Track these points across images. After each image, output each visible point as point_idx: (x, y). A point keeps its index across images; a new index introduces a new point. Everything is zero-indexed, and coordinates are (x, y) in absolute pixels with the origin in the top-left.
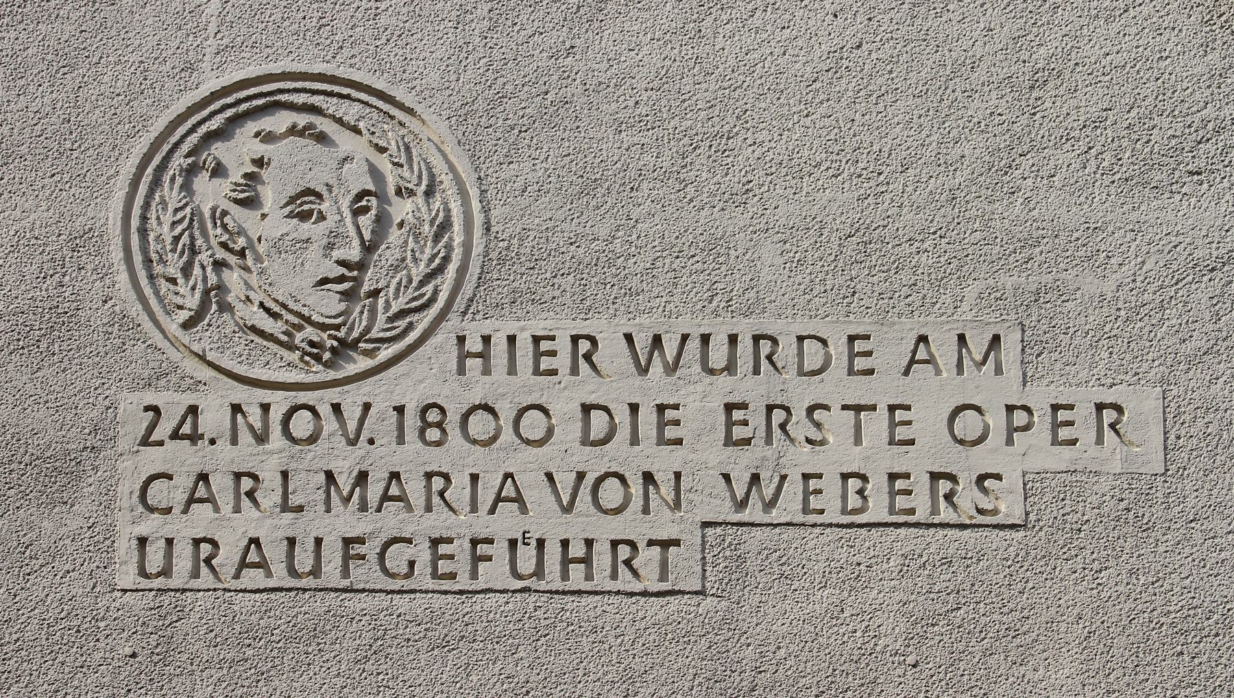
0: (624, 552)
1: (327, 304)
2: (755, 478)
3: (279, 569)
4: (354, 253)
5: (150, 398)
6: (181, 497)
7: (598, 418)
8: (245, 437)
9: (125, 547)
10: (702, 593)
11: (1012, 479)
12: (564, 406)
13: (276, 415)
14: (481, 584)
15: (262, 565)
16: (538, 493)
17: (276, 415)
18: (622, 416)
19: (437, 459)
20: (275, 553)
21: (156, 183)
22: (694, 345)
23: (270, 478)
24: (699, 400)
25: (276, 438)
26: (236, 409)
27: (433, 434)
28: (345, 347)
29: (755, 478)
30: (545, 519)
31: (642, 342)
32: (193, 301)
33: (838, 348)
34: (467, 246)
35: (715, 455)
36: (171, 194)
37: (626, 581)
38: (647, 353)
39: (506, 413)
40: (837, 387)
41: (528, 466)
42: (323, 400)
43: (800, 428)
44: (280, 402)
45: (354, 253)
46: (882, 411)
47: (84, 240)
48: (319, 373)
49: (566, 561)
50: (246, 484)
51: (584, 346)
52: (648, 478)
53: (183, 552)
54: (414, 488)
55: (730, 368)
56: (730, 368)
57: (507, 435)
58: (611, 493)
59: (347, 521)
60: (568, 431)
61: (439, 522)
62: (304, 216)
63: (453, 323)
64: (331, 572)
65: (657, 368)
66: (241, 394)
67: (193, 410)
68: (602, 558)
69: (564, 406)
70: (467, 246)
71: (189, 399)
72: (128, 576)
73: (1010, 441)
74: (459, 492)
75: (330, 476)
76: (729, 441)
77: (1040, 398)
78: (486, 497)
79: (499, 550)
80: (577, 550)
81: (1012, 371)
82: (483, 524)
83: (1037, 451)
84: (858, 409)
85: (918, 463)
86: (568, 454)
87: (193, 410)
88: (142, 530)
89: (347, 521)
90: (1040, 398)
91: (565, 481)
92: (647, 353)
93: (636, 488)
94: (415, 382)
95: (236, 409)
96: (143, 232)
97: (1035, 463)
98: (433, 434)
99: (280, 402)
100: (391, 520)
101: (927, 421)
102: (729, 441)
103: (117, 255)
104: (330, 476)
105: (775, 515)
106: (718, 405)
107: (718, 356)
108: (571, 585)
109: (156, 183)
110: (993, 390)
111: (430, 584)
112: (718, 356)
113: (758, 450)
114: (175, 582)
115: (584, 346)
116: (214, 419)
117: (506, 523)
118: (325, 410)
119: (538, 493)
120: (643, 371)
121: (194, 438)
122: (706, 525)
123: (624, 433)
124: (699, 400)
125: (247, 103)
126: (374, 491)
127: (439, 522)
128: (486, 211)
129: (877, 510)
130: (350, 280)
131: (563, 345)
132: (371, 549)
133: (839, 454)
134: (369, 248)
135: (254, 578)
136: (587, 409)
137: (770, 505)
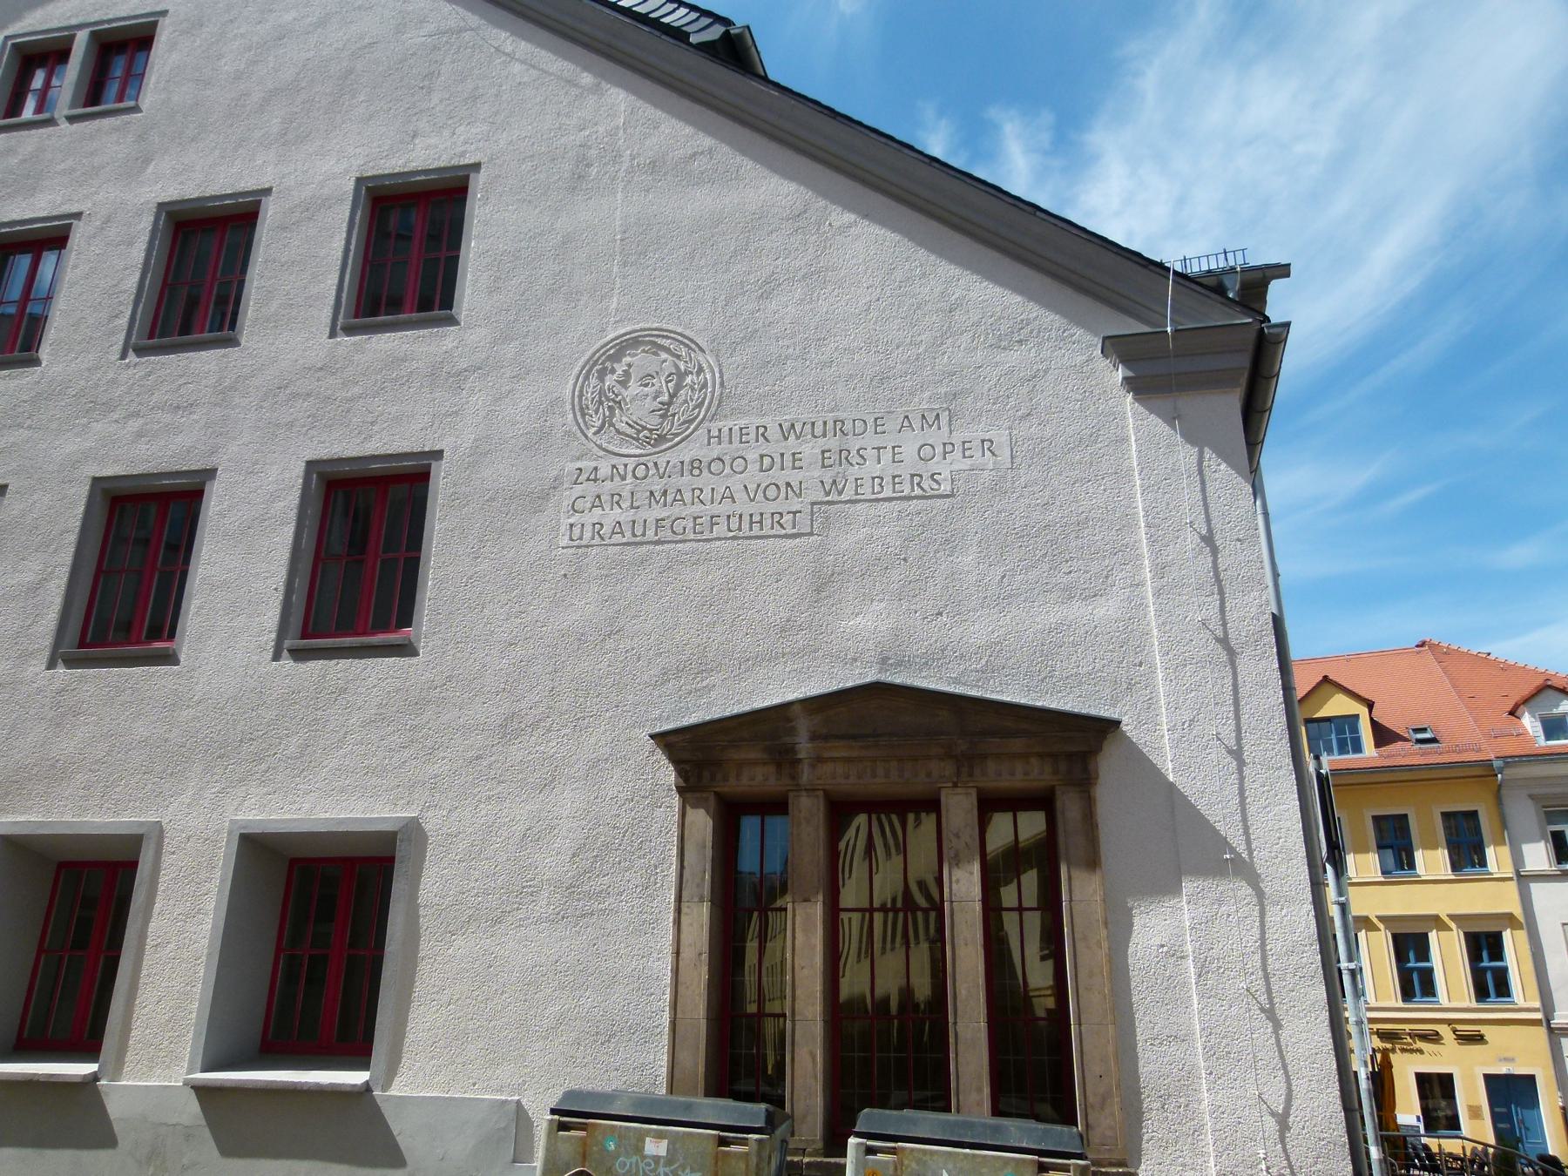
0: (777, 518)
1: (652, 422)
2: (834, 482)
3: (628, 534)
4: (666, 398)
5: (579, 465)
6: (589, 505)
7: (767, 461)
8: (617, 479)
9: (563, 528)
10: (811, 534)
11: (946, 474)
12: (752, 456)
13: (630, 468)
14: (715, 535)
15: (622, 533)
16: (740, 496)
17: (630, 468)
18: (777, 459)
19: (698, 482)
20: (627, 529)
21: (587, 378)
22: (808, 426)
23: (626, 494)
24: (810, 450)
25: (629, 479)
26: (614, 466)
27: (696, 472)
28: (662, 438)
29: (834, 482)
30: (743, 506)
31: (786, 426)
32: (598, 424)
33: (870, 422)
34: (713, 392)
35: (817, 473)
36: (593, 381)
37: (778, 531)
38: (787, 431)
39: (727, 459)
40: (870, 440)
41: (736, 484)
42: (650, 461)
43: (855, 459)
44: (631, 462)
45: (666, 398)
46: (889, 448)
47: (557, 401)
48: (650, 449)
49: (751, 523)
50: (616, 498)
51: (761, 430)
52: (788, 484)
53: (588, 528)
54: (687, 496)
55: (824, 435)
56: (824, 435)
57: (727, 470)
58: (772, 492)
59: (659, 512)
60: (753, 468)
61: (697, 509)
62: (646, 385)
63: (706, 424)
64: (650, 533)
65: (792, 437)
66: (616, 460)
67: (596, 469)
68: (767, 522)
69: (752, 456)
70: (713, 392)
71: (594, 464)
72: (565, 541)
73: (123, 356)
74: (706, 496)
75: (652, 493)
76: (823, 466)
77: (957, 438)
78: (718, 497)
79: (723, 520)
80: (756, 518)
81: (945, 429)
82: (717, 509)
83: (957, 462)
84: (879, 449)
85: (905, 471)
86: (753, 476)
87: (596, 469)
88: (571, 521)
89: (659, 512)
90: (957, 438)
91: (752, 487)
92: (787, 431)
93: (783, 489)
94: (687, 453)
95: (614, 466)
96: (581, 396)
97: (955, 467)
98: (696, 472)
99: (631, 462)
100: (677, 510)
101: (909, 451)
102: (823, 466)
103: (568, 407)
104: (652, 493)
105: (844, 497)
106: (818, 451)
107: (818, 430)
108: (753, 533)
109: (587, 378)
110: (937, 436)
111: (692, 536)
112: (818, 430)
113: (837, 469)
114: (584, 542)
115: (761, 430)
116: (604, 470)
117: (725, 508)
118: (650, 465)
119: (740, 496)
120: (786, 439)
121: (595, 480)
122: (813, 504)
123: (777, 465)
124: (810, 450)
125: (630, 343)
126: (669, 498)
127: (697, 509)
128: (721, 377)
129: (887, 493)
130: (665, 411)
131: (752, 430)
132: (667, 523)
133: (872, 468)
134: (672, 396)
135: (617, 538)
136: (762, 456)
137: (840, 493)
